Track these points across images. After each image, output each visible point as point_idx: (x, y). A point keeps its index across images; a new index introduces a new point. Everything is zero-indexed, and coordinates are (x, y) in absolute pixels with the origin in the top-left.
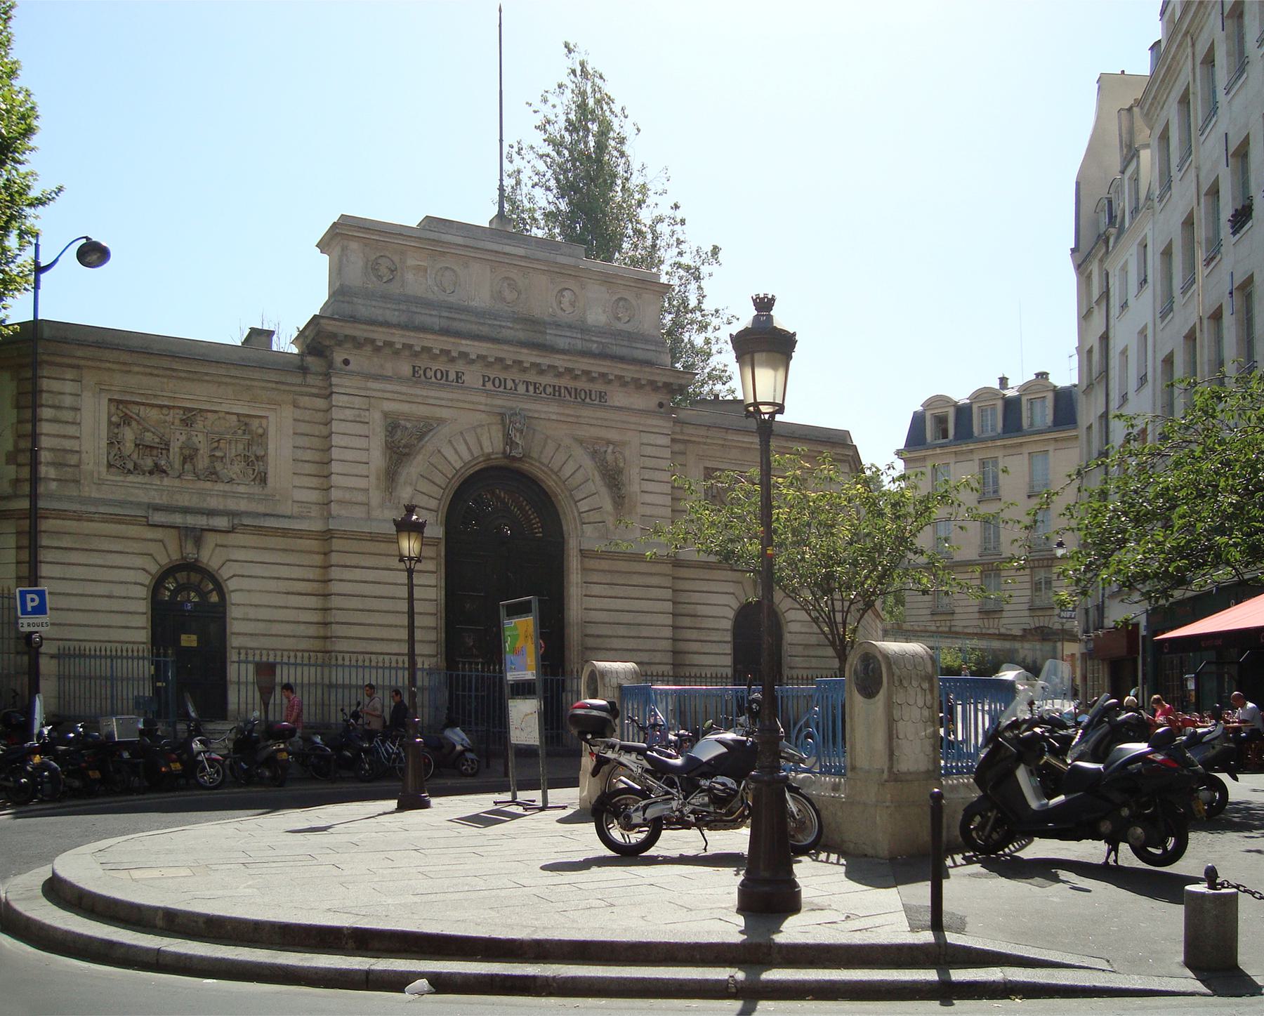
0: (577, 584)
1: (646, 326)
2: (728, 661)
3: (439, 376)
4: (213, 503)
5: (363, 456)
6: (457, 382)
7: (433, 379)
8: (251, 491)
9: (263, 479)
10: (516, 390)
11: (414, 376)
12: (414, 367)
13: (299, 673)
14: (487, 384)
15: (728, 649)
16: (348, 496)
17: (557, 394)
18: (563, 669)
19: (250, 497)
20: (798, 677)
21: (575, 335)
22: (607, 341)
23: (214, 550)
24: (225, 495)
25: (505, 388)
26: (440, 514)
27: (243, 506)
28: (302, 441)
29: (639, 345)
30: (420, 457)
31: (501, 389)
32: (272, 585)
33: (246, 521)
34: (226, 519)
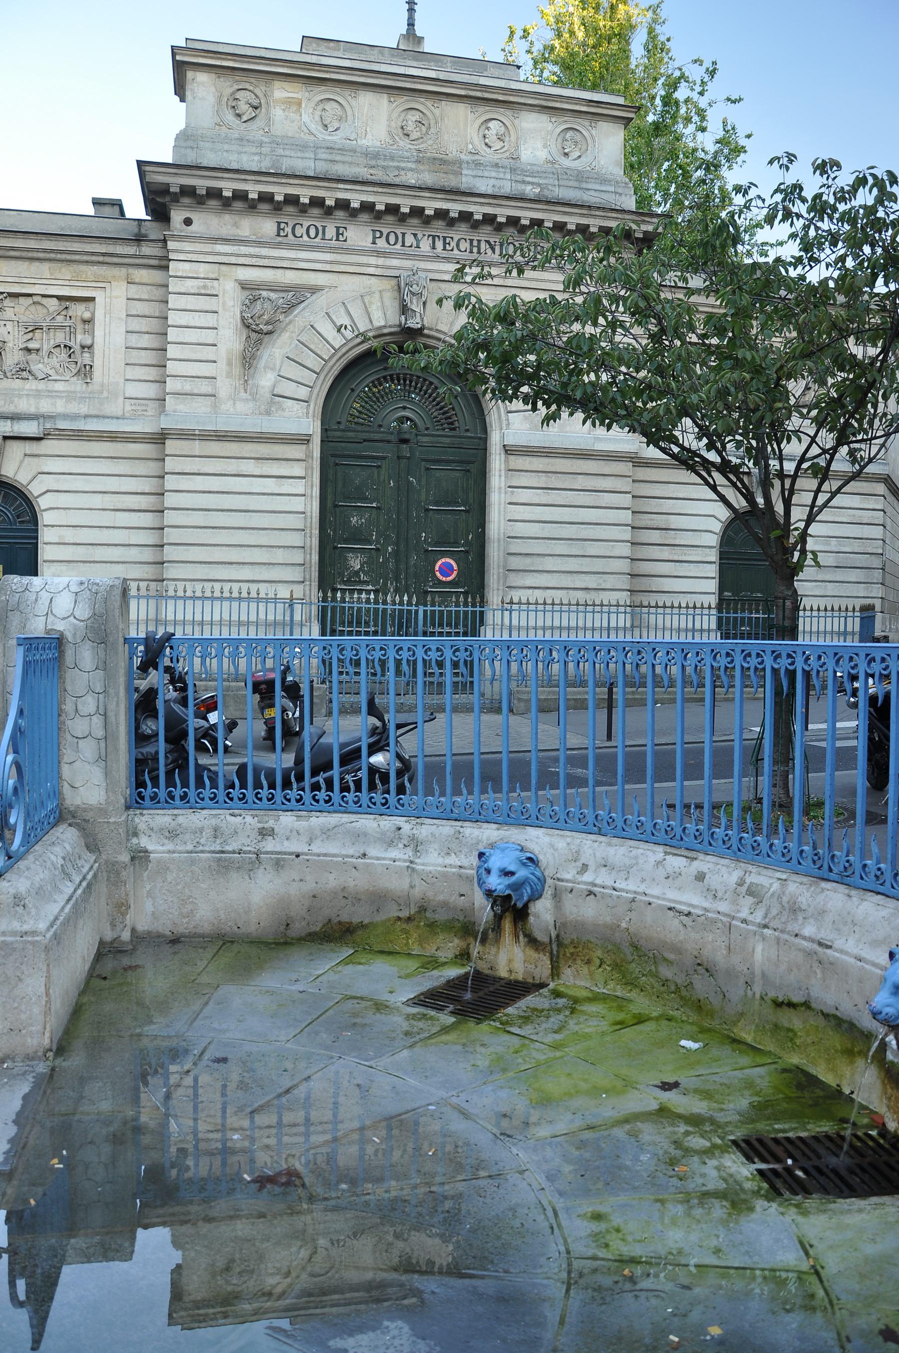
0: (500, 488)
1: (602, 163)
2: (712, 586)
3: (312, 232)
4: (24, 406)
5: (208, 336)
6: (337, 240)
7: (305, 237)
8: (72, 388)
9: (86, 372)
10: (418, 247)
11: (278, 235)
12: (279, 223)
13: (208, 609)
14: (377, 241)
15: (713, 570)
16: (188, 387)
17: (475, 250)
18: (482, 597)
19: (70, 396)
20: (847, 609)
21: (501, 176)
22: (546, 181)
23: (21, 462)
24: (38, 394)
25: (403, 245)
26: (312, 406)
27: (60, 407)
28: (136, 324)
29: (590, 186)
30: (285, 336)
31: (398, 246)
32: (97, 501)
33: (62, 425)
34: (35, 423)
